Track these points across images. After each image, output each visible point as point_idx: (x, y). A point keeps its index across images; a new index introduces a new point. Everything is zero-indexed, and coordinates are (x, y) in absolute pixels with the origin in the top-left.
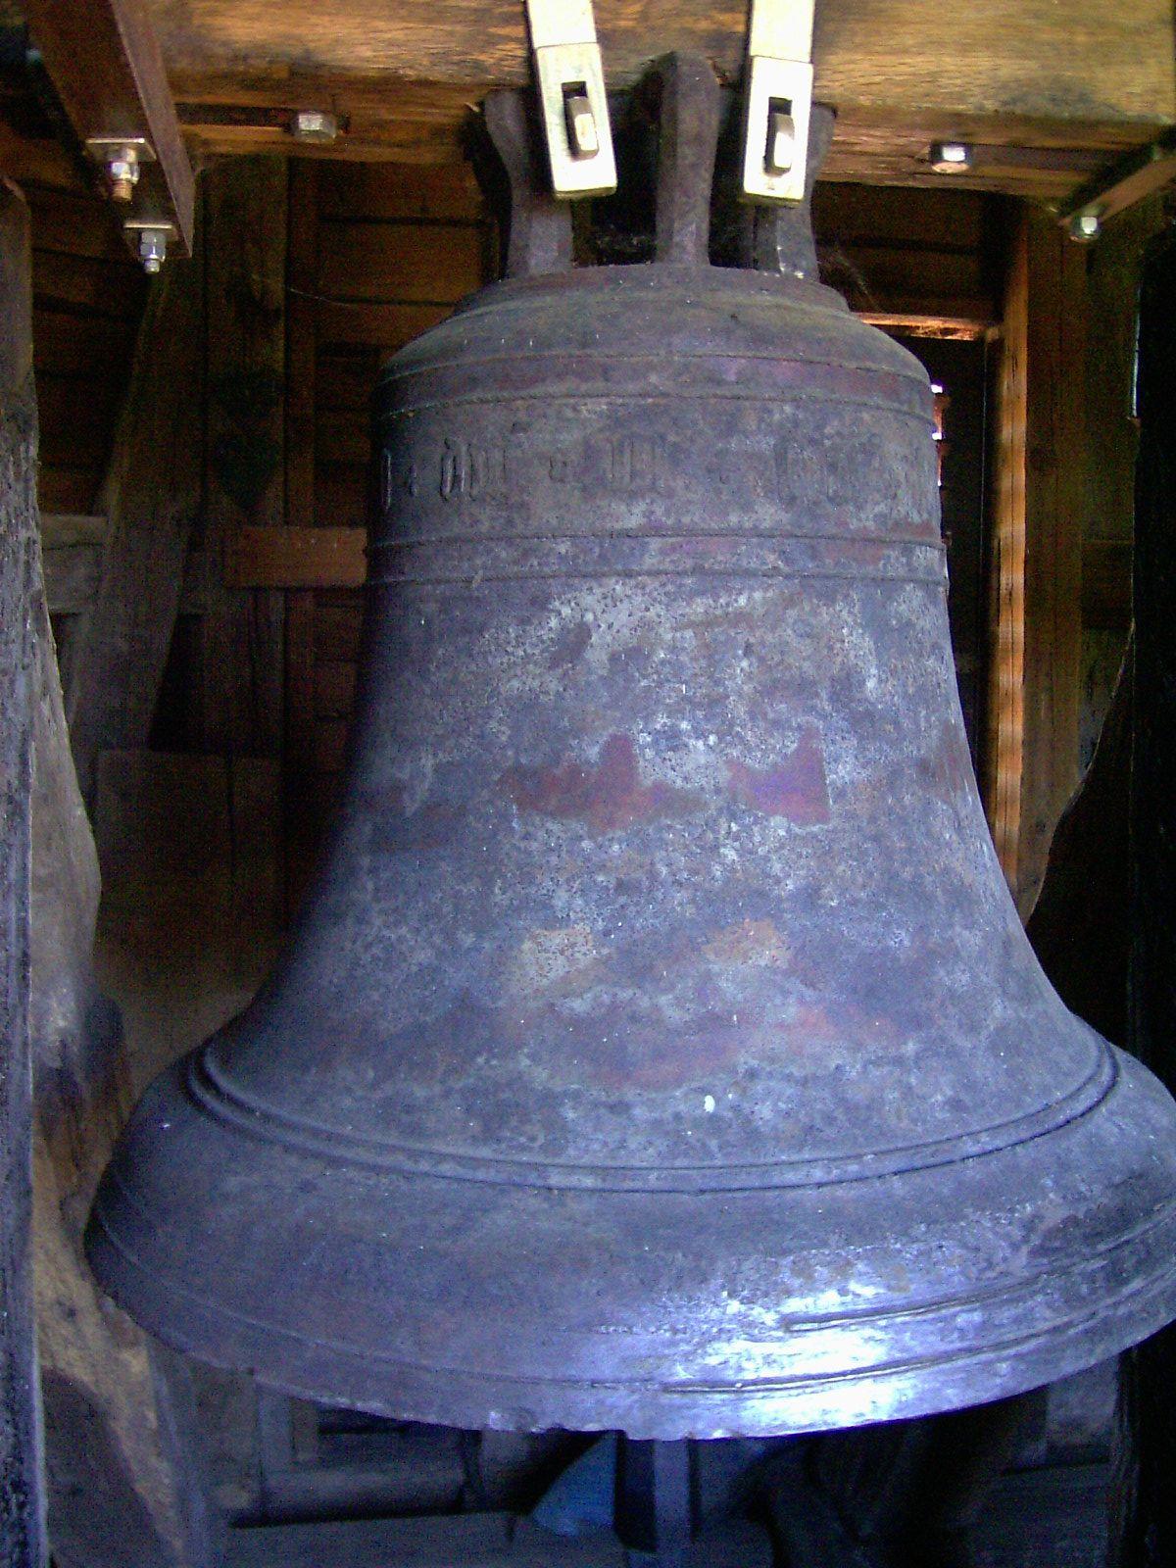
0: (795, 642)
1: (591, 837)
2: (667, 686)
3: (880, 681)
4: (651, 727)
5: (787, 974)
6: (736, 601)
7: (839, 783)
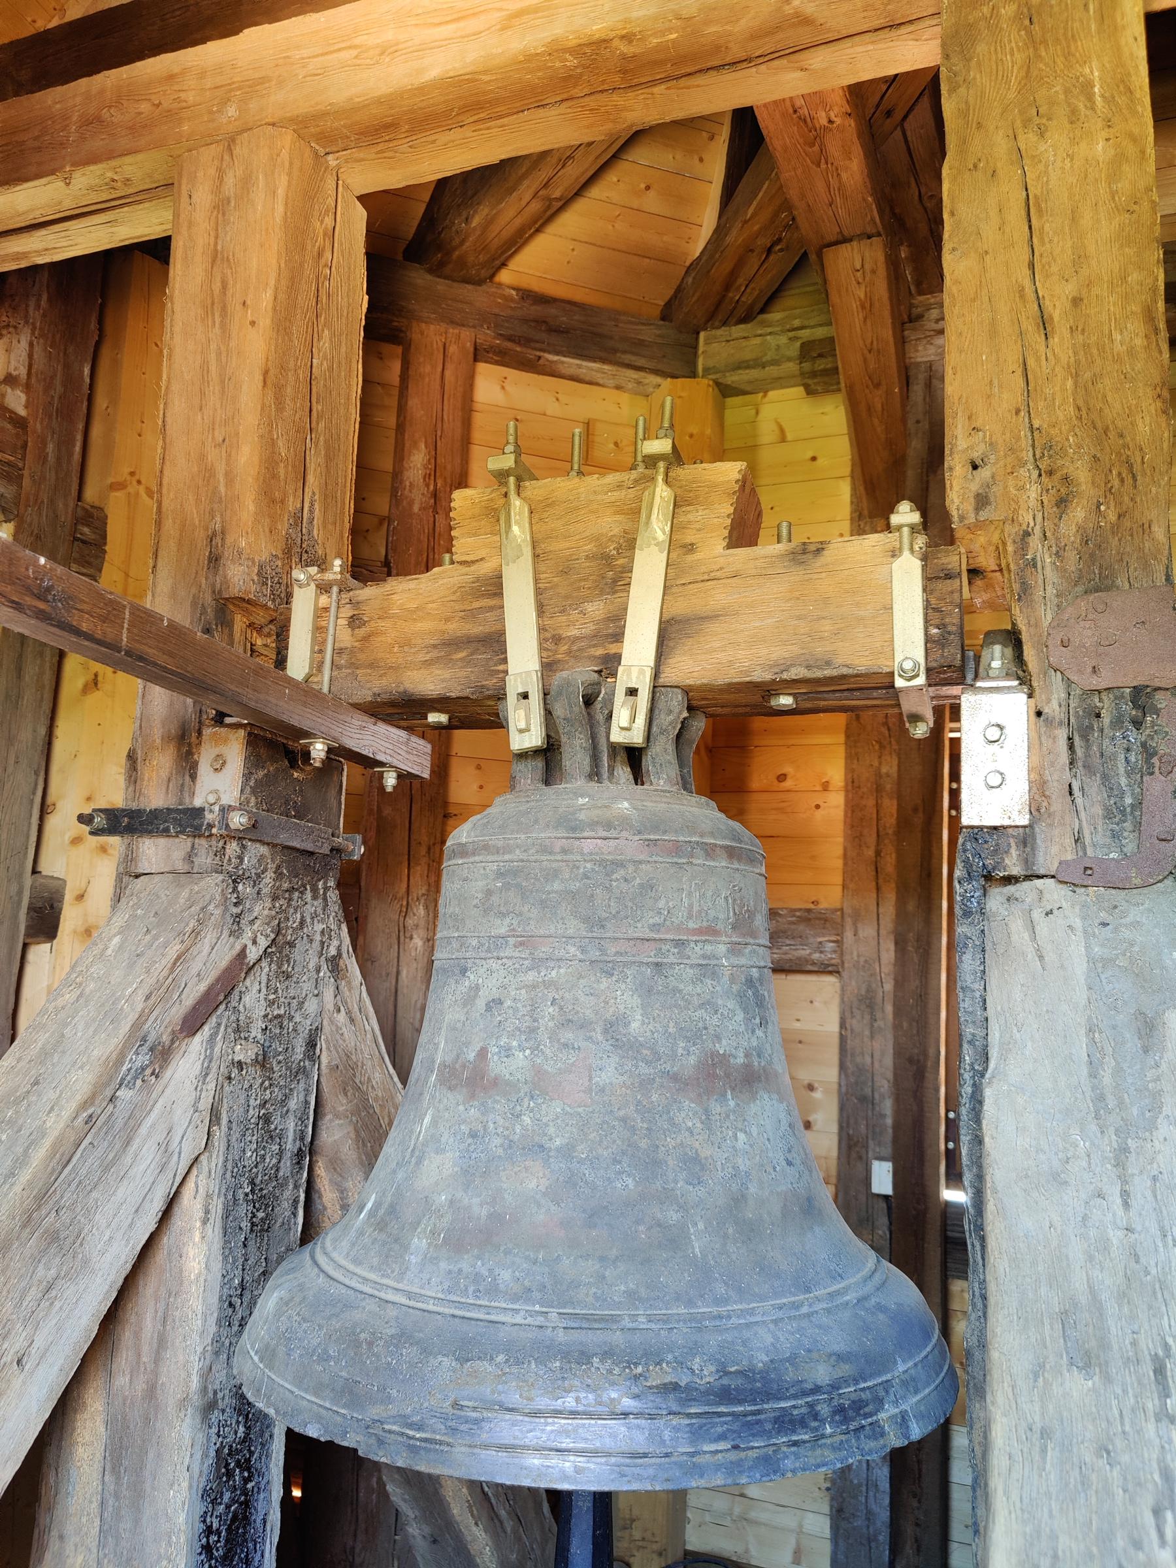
0: (582, 998)
1: (464, 1104)
3: (643, 1023)
5: (544, 1194)
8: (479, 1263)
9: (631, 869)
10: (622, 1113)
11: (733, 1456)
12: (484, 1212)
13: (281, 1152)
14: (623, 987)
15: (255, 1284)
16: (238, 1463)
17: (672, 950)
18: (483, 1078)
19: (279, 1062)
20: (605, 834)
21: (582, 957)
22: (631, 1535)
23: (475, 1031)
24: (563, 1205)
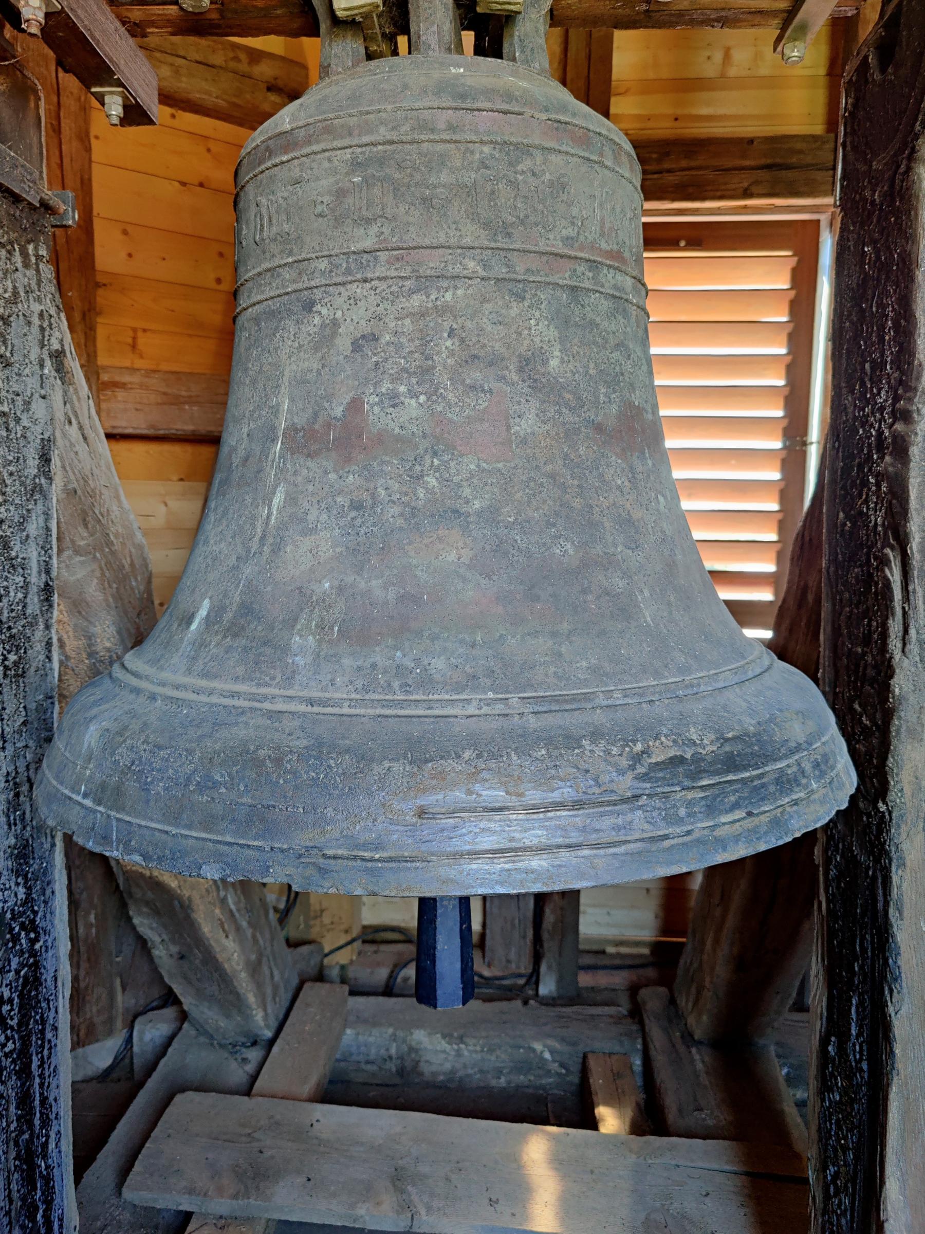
0: (488, 327)
1: (336, 471)
2: (390, 361)
4: (378, 391)
5: (469, 567)
6: (443, 297)
7: (522, 433)
8: (399, 654)
9: (539, 159)
10: (549, 468)
11: (749, 823)
12: (391, 595)
13: (26, 585)
14: (537, 314)
15: (16, 736)
16: (23, 927)
17: (587, 273)
18: (360, 436)
19: (11, 474)
20: (505, 107)
21: (484, 274)
22: (322, 922)
23: (339, 378)
24: (495, 578)
